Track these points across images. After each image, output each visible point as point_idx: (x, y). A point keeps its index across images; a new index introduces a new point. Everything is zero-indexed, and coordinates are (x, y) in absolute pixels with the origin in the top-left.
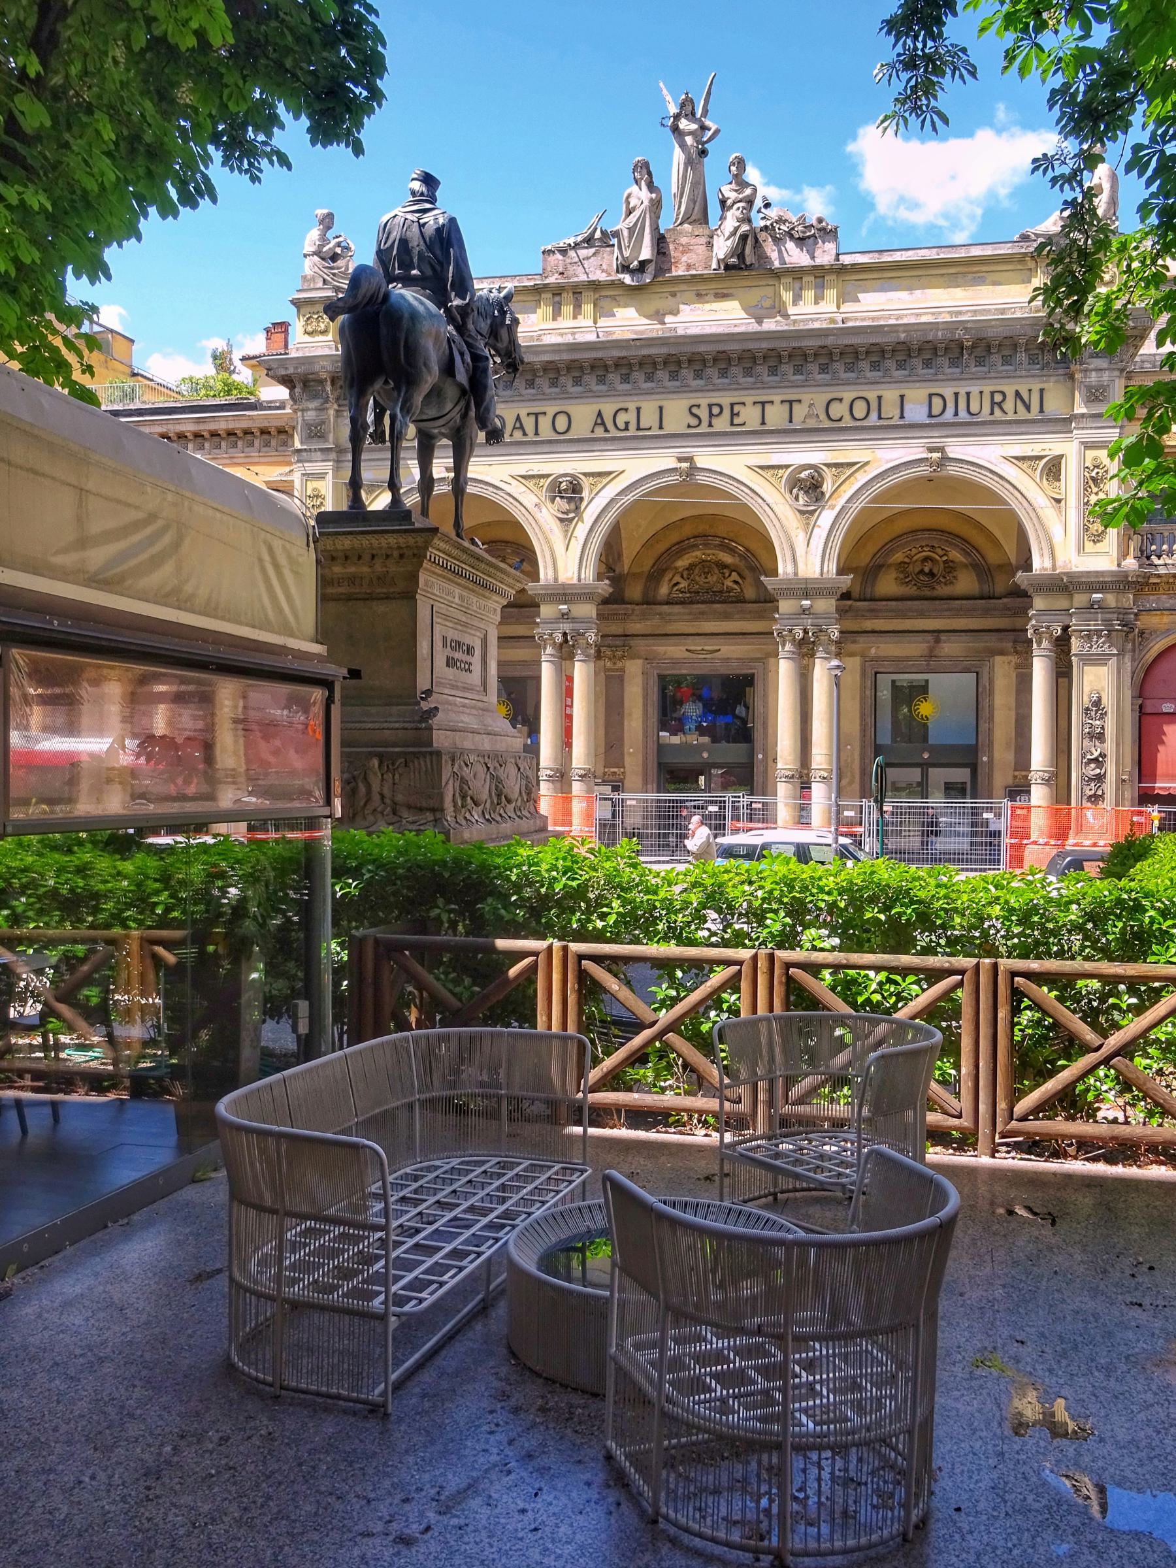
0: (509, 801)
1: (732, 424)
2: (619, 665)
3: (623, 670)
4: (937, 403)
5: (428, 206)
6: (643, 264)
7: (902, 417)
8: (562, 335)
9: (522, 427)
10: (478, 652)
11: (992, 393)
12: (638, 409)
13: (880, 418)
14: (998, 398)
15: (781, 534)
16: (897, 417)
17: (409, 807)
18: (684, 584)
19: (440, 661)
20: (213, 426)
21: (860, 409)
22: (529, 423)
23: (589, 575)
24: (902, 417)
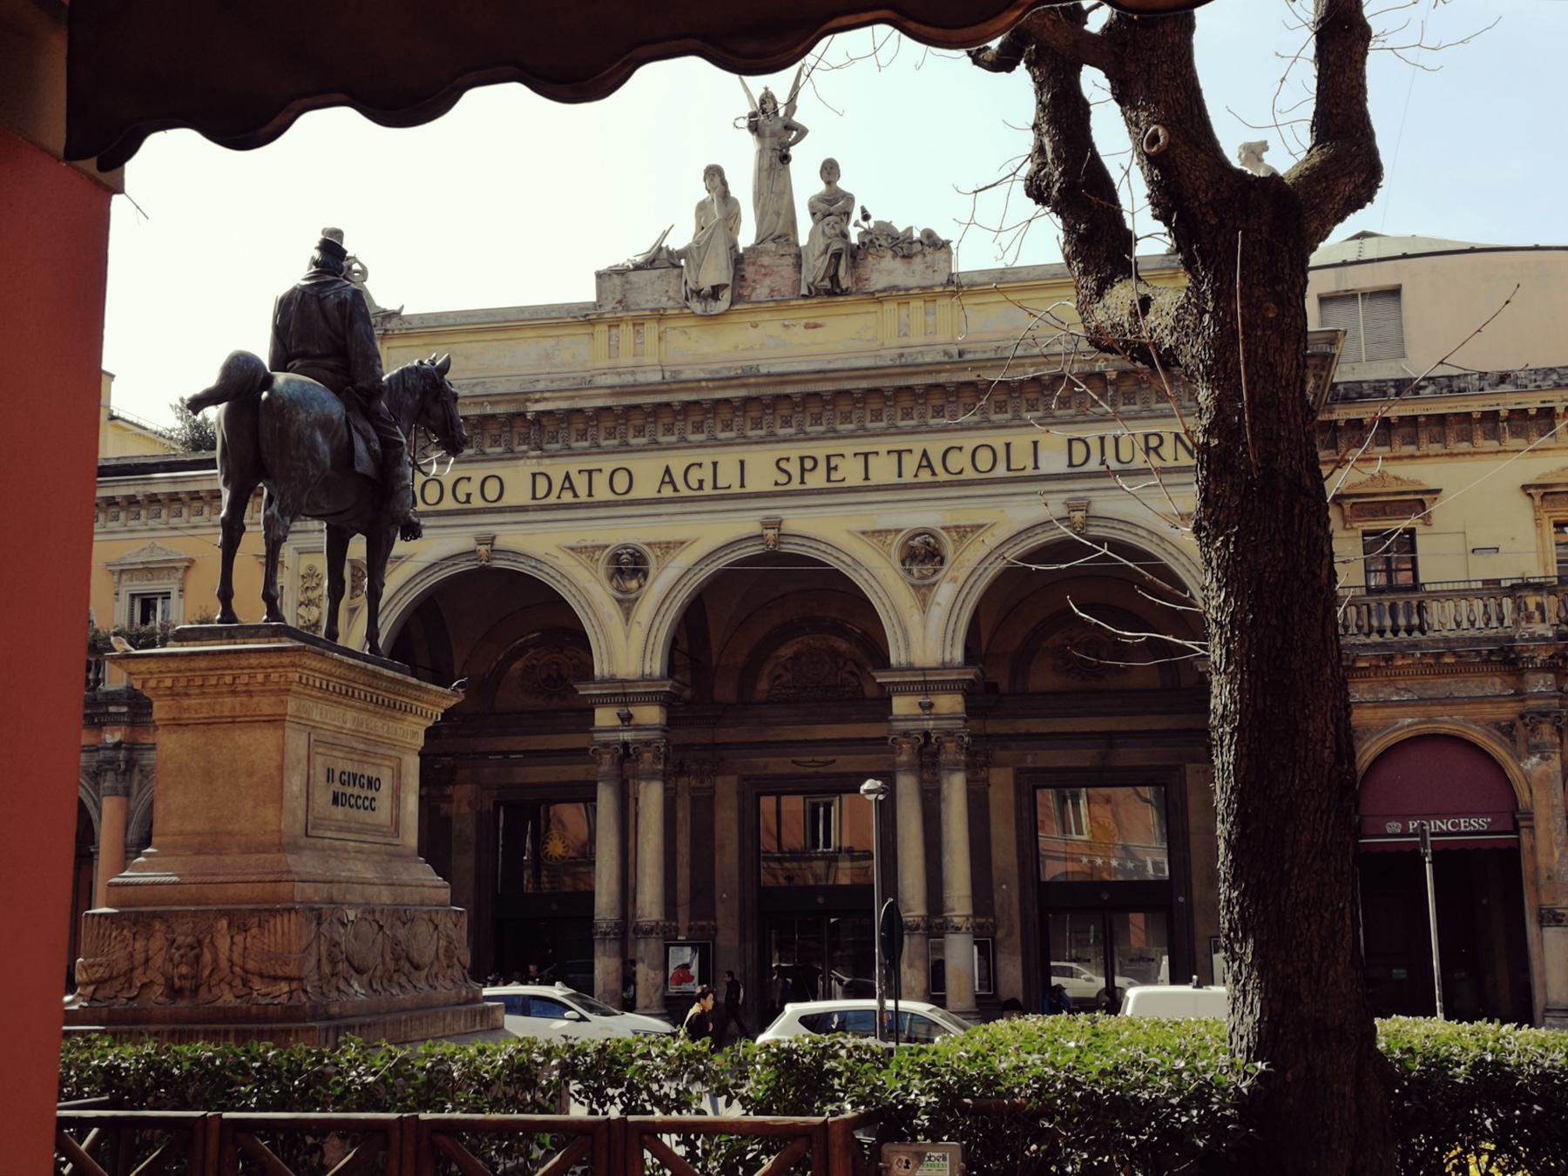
0: (417, 967)
1: (829, 480)
2: (983, 775)
3: (712, 788)
4: (1079, 449)
5: (330, 278)
6: (715, 292)
7: (1036, 467)
8: (619, 374)
9: (572, 488)
10: (386, 786)
11: (1147, 436)
12: (715, 464)
13: (1009, 469)
14: (1154, 442)
15: (892, 614)
16: (1032, 465)
17: (261, 976)
18: (787, 677)
19: (322, 797)
20: (193, 487)
21: (984, 459)
22: (580, 483)
23: (656, 666)
24: (1036, 467)
